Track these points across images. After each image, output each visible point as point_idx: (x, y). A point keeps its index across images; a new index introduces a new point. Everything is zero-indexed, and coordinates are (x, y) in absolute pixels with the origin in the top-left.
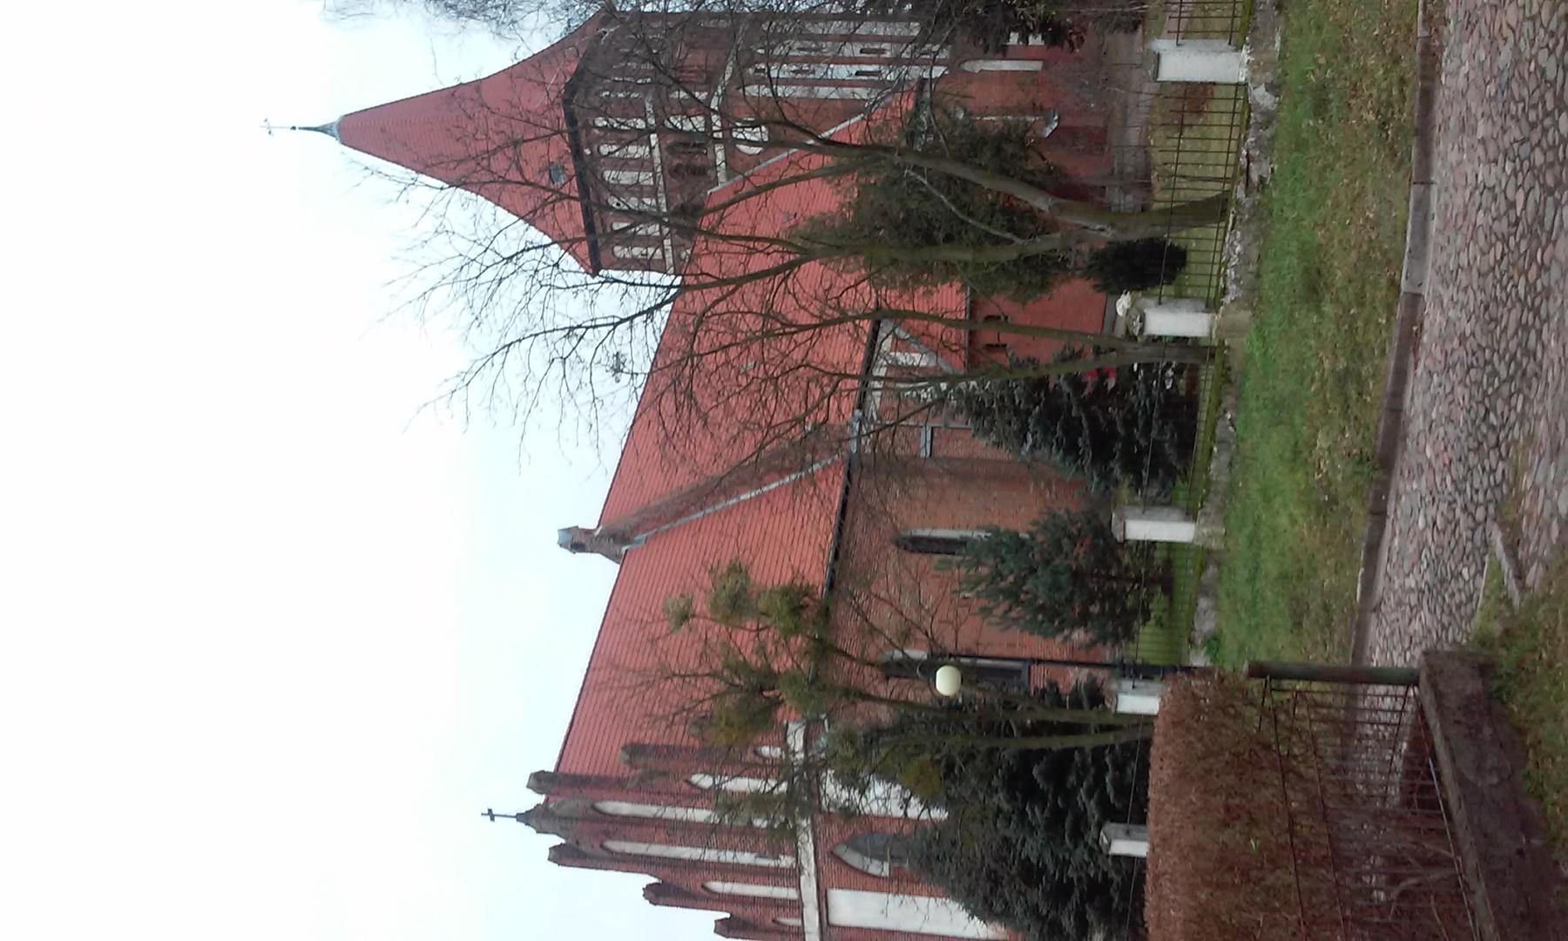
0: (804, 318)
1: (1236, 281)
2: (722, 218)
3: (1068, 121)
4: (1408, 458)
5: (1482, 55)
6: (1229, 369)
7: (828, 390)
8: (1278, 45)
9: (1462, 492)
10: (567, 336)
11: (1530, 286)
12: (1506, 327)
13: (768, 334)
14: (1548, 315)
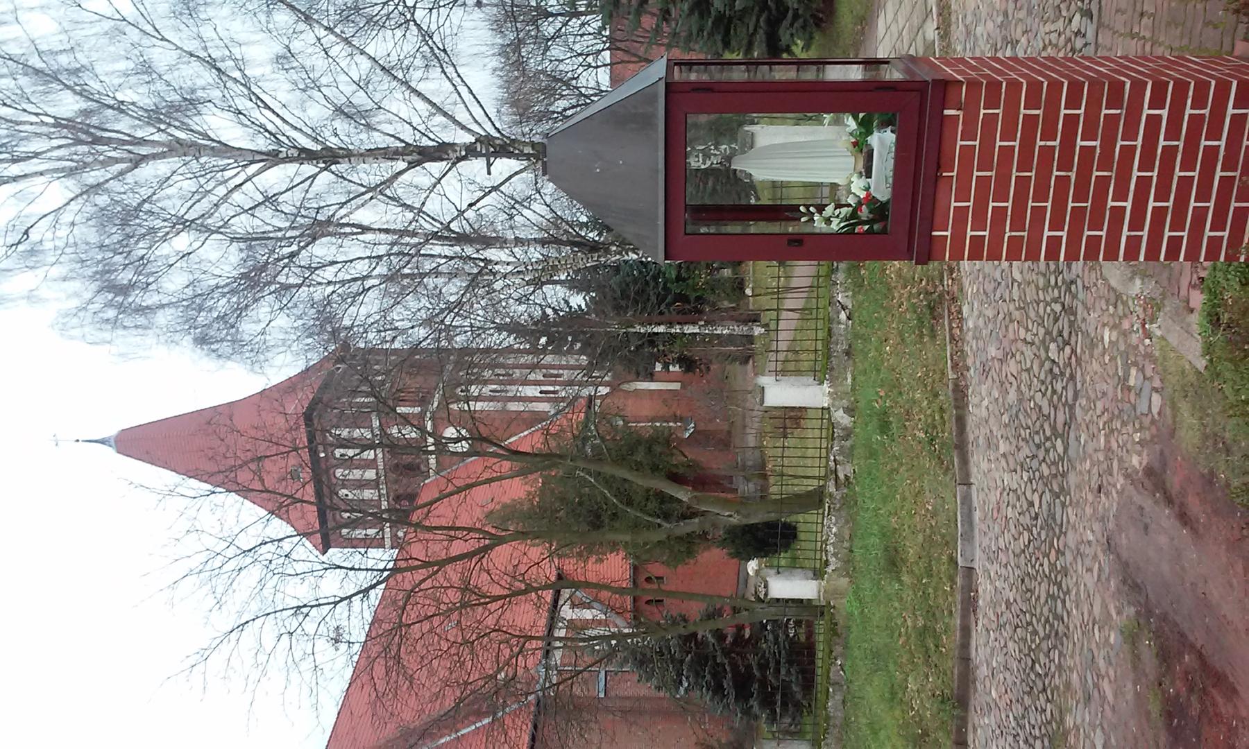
0: (497, 591)
1: (835, 555)
2: (429, 512)
3: (702, 427)
4: (978, 699)
5: (996, 394)
6: (836, 624)
7: (516, 650)
8: (849, 380)
9: (1022, 727)
10: (295, 614)
11: (1052, 566)
12: (1039, 597)
13: (464, 605)
14: (1068, 589)
